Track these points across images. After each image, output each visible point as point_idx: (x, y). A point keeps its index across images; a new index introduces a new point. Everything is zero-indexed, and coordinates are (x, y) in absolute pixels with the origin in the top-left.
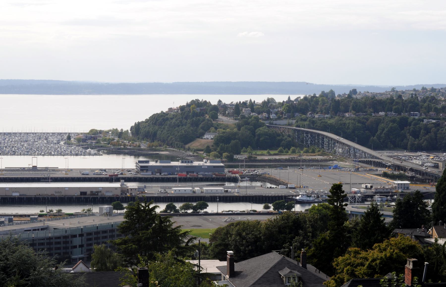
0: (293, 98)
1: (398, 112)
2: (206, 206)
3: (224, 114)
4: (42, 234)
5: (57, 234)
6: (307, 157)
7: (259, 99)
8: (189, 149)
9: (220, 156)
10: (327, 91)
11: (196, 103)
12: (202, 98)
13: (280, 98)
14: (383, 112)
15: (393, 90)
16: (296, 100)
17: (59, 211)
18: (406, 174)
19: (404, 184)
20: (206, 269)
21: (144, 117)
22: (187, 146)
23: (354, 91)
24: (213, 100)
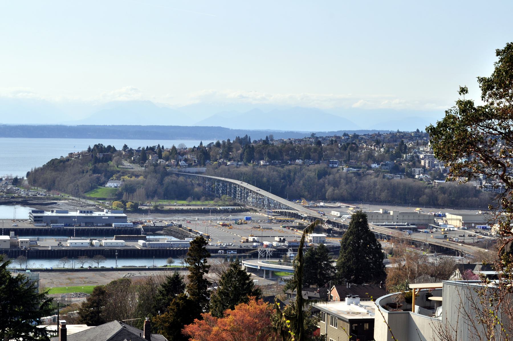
0: (205, 143)
10: (242, 136)
11: (99, 148)
12: (106, 143)
14: (300, 160)
15: (313, 135)
17: (156, 207)
19: (320, 237)
24: (118, 145)
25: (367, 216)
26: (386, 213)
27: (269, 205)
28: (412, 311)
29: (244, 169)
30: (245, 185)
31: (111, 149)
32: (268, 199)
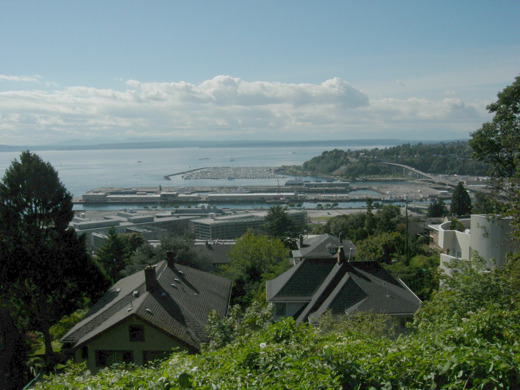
0: (388, 147)
1: (443, 154)
2: (337, 205)
3: (351, 157)
4: (249, 220)
5: (258, 220)
6: (442, 181)
7: (370, 148)
8: (332, 175)
9: (347, 178)
10: (406, 143)
11: (336, 150)
12: (339, 148)
13: (381, 147)
15: (442, 142)
16: (390, 148)
17: (262, 208)
18: (446, 187)
20: (177, 288)
21: (309, 158)
22: (331, 174)
23: (421, 144)
24: (345, 149)
25: (20, 156)
26: (478, 180)
27: (420, 176)
28: (470, 220)
29: (407, 160)
30: (406, 167)
31: (341, 151)
32: (419, 174)
